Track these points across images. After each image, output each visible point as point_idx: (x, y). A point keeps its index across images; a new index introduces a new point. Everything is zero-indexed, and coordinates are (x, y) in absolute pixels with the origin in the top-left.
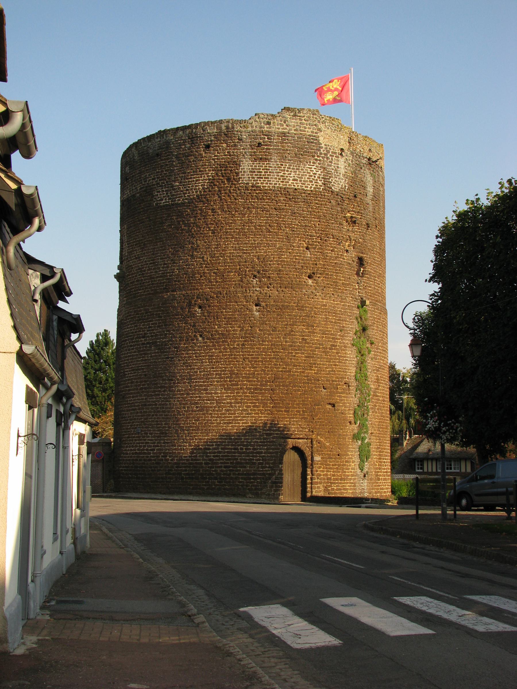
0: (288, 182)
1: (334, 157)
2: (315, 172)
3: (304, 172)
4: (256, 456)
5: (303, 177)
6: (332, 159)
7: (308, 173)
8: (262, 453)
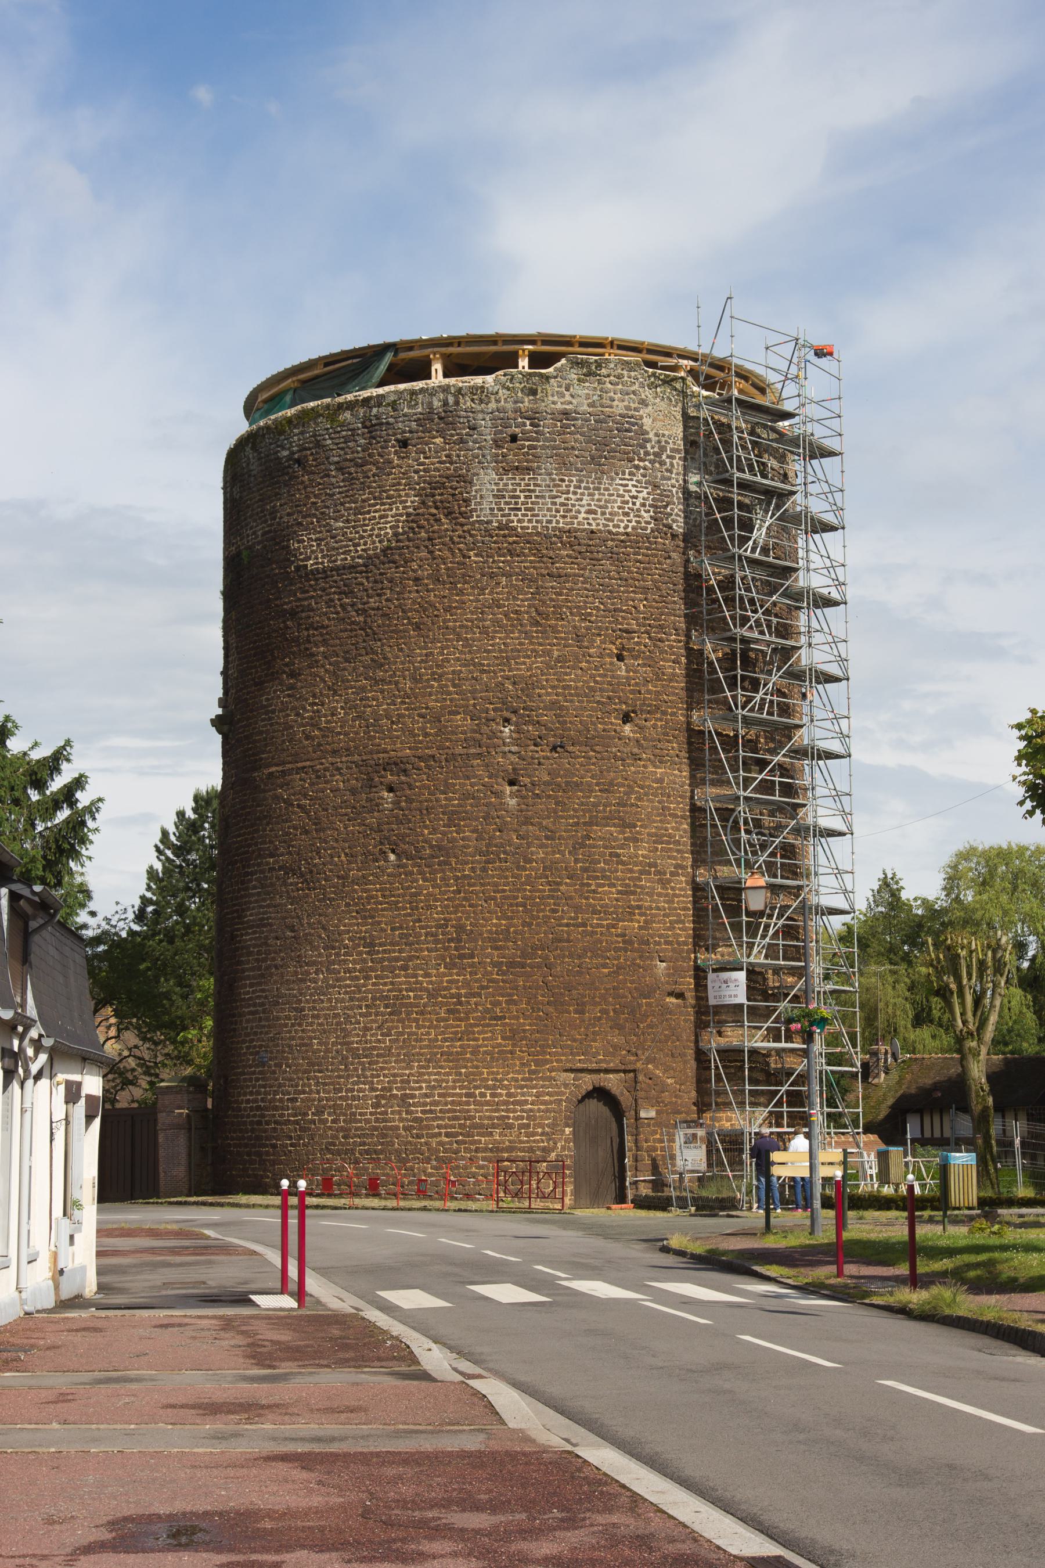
4: (515, 1111)
7: (619, 496)
8: (526, 1102)
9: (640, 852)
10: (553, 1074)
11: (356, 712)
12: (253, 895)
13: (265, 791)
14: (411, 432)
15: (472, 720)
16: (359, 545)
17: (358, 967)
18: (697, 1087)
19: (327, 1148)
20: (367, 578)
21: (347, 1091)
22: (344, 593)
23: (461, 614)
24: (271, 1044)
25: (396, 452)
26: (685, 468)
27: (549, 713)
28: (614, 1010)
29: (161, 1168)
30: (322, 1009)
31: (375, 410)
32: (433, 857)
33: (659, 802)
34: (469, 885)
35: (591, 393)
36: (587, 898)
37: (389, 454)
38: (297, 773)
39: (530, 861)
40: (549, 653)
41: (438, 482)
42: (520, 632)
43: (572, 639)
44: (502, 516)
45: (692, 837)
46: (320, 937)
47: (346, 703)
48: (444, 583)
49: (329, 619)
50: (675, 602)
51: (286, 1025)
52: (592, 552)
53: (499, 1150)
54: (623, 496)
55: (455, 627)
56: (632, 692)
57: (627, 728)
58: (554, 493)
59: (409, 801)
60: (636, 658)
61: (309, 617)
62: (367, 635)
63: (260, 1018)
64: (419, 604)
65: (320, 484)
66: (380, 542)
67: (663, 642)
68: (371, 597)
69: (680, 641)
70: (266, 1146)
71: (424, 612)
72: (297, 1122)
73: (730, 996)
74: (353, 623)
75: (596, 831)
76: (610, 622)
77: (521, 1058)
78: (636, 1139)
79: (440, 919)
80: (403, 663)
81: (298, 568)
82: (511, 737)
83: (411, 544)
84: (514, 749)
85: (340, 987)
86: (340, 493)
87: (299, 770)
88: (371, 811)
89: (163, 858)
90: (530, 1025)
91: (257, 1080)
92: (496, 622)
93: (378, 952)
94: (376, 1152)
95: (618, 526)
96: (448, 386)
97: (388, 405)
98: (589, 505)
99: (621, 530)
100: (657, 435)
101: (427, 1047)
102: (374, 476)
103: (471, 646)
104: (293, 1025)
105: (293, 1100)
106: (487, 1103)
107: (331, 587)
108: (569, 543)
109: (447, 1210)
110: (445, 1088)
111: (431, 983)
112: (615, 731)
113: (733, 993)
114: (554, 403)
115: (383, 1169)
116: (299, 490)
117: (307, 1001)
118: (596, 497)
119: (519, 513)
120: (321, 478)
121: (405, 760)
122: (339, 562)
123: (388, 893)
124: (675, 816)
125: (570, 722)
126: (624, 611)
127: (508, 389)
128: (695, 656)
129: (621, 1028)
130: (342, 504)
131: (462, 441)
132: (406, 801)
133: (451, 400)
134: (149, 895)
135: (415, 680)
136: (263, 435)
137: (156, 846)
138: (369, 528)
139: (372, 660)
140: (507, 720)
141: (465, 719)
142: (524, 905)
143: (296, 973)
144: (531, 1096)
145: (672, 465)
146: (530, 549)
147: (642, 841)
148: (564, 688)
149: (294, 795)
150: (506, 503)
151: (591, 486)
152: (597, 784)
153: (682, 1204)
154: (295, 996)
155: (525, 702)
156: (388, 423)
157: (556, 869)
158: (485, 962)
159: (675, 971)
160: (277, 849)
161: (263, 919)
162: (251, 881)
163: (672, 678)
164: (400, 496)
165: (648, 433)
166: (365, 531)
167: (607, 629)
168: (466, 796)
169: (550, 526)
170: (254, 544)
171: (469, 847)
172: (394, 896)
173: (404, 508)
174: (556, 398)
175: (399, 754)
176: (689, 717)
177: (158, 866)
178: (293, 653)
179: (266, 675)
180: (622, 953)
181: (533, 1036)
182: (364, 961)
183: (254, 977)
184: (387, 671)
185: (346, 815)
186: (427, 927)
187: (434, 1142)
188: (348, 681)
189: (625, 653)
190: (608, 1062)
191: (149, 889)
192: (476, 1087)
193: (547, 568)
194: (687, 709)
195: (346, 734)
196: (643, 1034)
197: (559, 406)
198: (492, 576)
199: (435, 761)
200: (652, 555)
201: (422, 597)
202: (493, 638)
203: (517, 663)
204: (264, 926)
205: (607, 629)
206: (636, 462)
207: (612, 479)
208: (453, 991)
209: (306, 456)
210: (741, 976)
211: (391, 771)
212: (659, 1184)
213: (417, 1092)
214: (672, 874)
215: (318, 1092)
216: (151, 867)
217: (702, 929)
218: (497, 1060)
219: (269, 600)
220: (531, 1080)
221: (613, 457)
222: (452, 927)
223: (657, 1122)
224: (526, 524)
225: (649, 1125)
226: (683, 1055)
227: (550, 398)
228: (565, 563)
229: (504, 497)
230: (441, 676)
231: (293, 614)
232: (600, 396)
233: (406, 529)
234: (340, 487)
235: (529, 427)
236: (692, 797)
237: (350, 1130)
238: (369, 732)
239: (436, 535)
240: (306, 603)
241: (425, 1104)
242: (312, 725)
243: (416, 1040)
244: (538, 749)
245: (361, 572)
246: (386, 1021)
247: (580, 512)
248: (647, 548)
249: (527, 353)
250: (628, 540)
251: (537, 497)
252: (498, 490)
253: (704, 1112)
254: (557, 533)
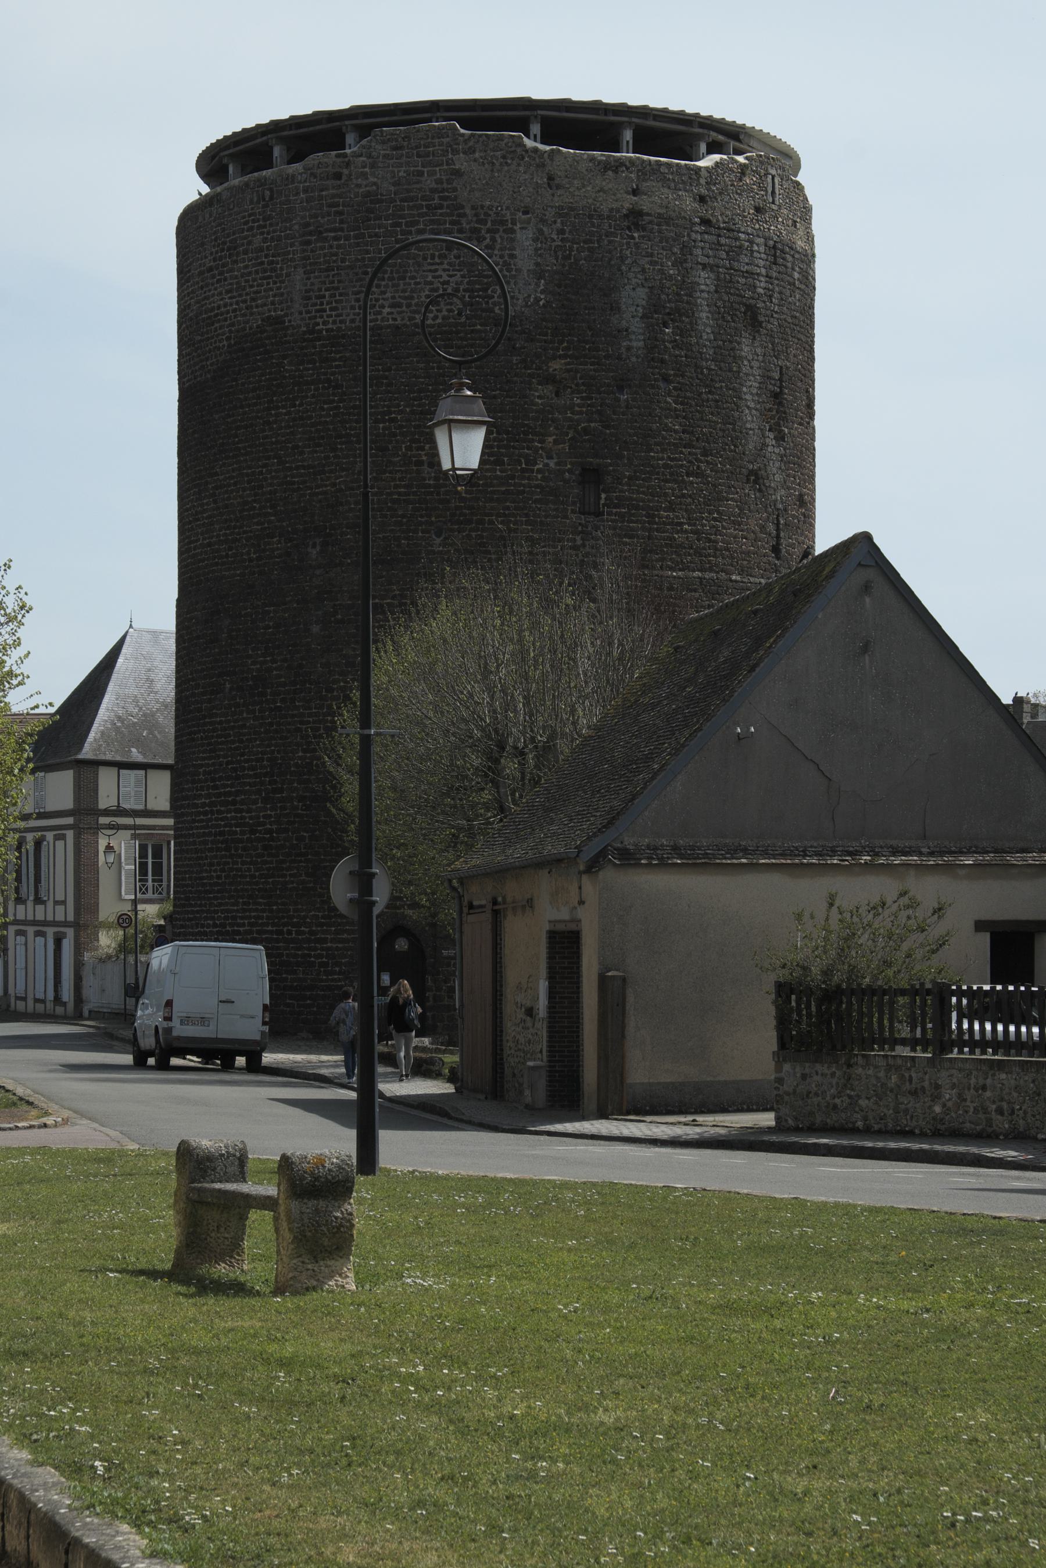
0: (380, 313)
1: (501, 233)
2: (445, 278)
3: (416, 284)
4: (315, 949)
5: (415, 295)
6: (493, 240)
7: (427, 283)
8: (325, 941)
224: (330, 326)
227: (355, 181)
247: (383, 307)
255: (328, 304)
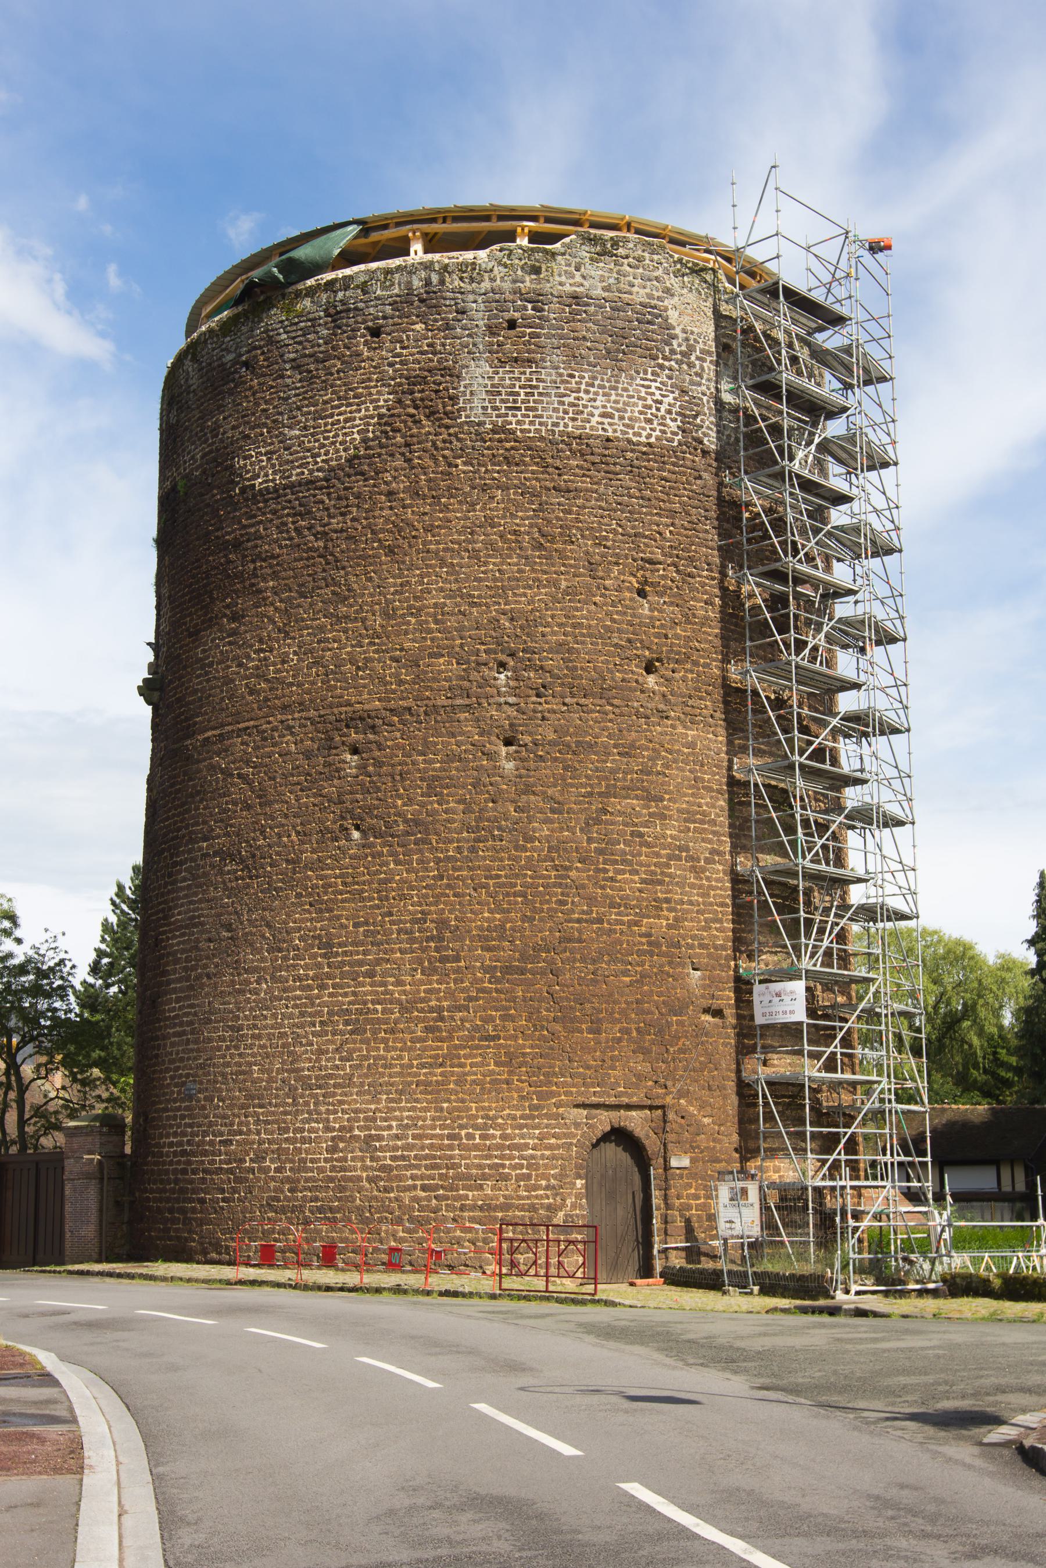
2: (658, 397)
5: (629, 409)
8: (526, 1146)
9: (668, 832)
10: (561, 1110)
11: (313, 657)
12: (182, 889)
13: (199, 761)
14: (384, 318)
15: (458, 663)
16: (319, 455)
17: (311, 973)
18: (740, 1128)
19: (268, 1204)
20: (329, 494)
21: (295, 1131)
22: (300, 514)
23: (445, 535)
24: (200, 1072)
25: (366, 343)
26: (718, 374)
27: (555, 656)
28: (638, 1030)
29: (67, 1227)
30: (265, 1027)
31: (340, 295)
32: (408, 833)
33: (690, 771)
34: (454, 869)
35: (606, 274)
36: (603, 888)
37: (357, 345)
38: (238, 736)
39: (532, 840)
40: (556, 584)
41: (418, 376)
42: (519, 556)
43: (584, 566)
44: (498, 416)
45: (730, 817)
46: (263, 936)
47: (300, 647)
48: (425, 496)
49: (281, 547)
50: (706, 531)
51: (219, 1049)
52: (607, 464)
53: (490, 1208)
54: (645, 400)
55: (438, 551)
56: (657, 635)
57: (651, 680)
58: (562, 391)
59: (378, 764)
60: (661, 595)
61: (256, 547)
62: (328, 563)
63: (188, 1039)
64: (393, 523)
65: (272, 387)
66: (345, 450)
67: (693, 577)
68: (333, 518)
69: (713, 579)
70: (192, 1200)
71: (399, 532)
72: (231, 1171)
73: (785, 1013)
74: (310, 549)
75: (613, 804)
76: (629, 549)
77: (519, 1090)
78: (666, 1195)
79: (417, 912)
80: (371, 595)
81: (243, 490)
82: (507, 685)
83: (383, 451)
84: (512, 700)
85: (287, 999)
86: (296, 395)
87: (240, 732)
88: (330, 778)
89: (118, 911)
90: (532, 1047)
91: (183, 1117)
92: (490, 545)
93: (337, 954)
94: (331, 1210)
95: (640, 435)
96: (432, 263)
97: (357, 287)
98: (604, 407)
99: (643, 439)
100: (684, 331)
101: (401, 1075)
102: (338, 372)
103: (458, 573)
104: (228, 1048)
105: (227, 1143)
106: (476, 1147)
107: (284, 509)
108: (580, 451)
109: (428, 1293)
110: (421, 1127)
111: (404, 992)
112: (637, 681)
113: (788, 1009)
114: (561, 284)
115: (341, 1231)
116: (246, 397)
117: (246, 1018)
118: (613, 398)
119: (519, 413)
120: (274, 380)
121: (373, 714)
122: (294, 478)
123: (350, 880)
124: (709, 789)
125: (582, 669)
126: (646, 537)
127: (505, 266)
128: (731, 600)
129: (646, 1052)
130: (299, 408)
131: (448, 327)
132: (374, 765)
133: (435, 278)
134: (103, 947)
135: (386, 615)
136: (206, 341)
137: (111, 899)
138: (331, 434)
139: (334, 593)
140: (502, 665)
141: (450, 663)
142: (524, 895)
143: (233, 982)
144: (533, 1138)
145: (702, 368)
146: (532, 457)
147: (671, 818)
148: (574, 626)
149: (233, 763)
150: (503, 401)
151: (607, 385)
152: (615, 746)
153: (740, 1281)
154: (231, 1012)
155: (525, 642)
156: (356, 309)
157: (565, 850)
158: (474, 967)
159: (712, 981)
160: (213, 830)
161: (193, 917)
162: (180, 872)
163: (705, 621)
164: (371, 394)
165: (674, 328)
166: (325, 438)
167: (626, 557)
168: (450, 758)
169: (557, 430)
170: (192, 470)
171: (453, 821)
172: (357, 883)
173: (376, 408)
174: (563, 279)
175: (367, 707)
176: (724, 670)
177: (113, 919)
178: (236, 592)
179: (203, 622)
180: (647, 958)
181: (536, 1061)
182: (319, 966)
183: (181, 990)
184: (352, 606)
185: (298, 784)
186: (400, 921)
187: (406, 1197)
188: (303, 620)
189: (648, 588)
190: (630, 1096)
191: (103, 940)
192: (461, 1127)
193: (553, 480)
194: (722, 661)
195: (300, 685)
196: (674, 1060)
197: (568, 288)
198: (484, 488)
199: (411, 715)
200: (679, 473)
201: (396, 515)
202: (486, 564)
203: (515, 595)
204: (195, 925)
205: (626, 557)
206: (660, 361)
207: (632, 378)
208: (433, 1003)
209: (255, 356)
210: (799, 987)
211: (356, 727)
212: (693, 1253)
213: (385, 1133)
214: (706, 860)
215: (258, 1133)
216: (106, 920)
217: (743, 931)
218: (489, 1092)
219: (208, 533)
220: (533, 1117)
221: (633, 353)
222: (432, 921)
223: (690, 1173)
224: (526, 427)
225: (681, 1177)
226: (722, 1088)
227: (557, 278)
228: (575, 475)
229: (499, 393)
230: (420, 610)
231: (237, 545)
232: (617, 279)
233: (378, 433)
234: (298, 388)
235: (530, 312)
236: (730, 768)
237: (299, 1181)
238: (329, 681)
239: (415, 440)
240: (252, 530)
241: (395, 1148)
242: (258, 676)
243: (385, 1066)
244: (542, 700)
245: (321, 489)
246: (347, 1042)
247: (593, 415)
248: (674, 464)
249: (526, 230)
250: (649, 451)
251: (540, 394)
252: (493, 386)
253: (748, 1160)
254: (565, 438)
255: (522, 403)
